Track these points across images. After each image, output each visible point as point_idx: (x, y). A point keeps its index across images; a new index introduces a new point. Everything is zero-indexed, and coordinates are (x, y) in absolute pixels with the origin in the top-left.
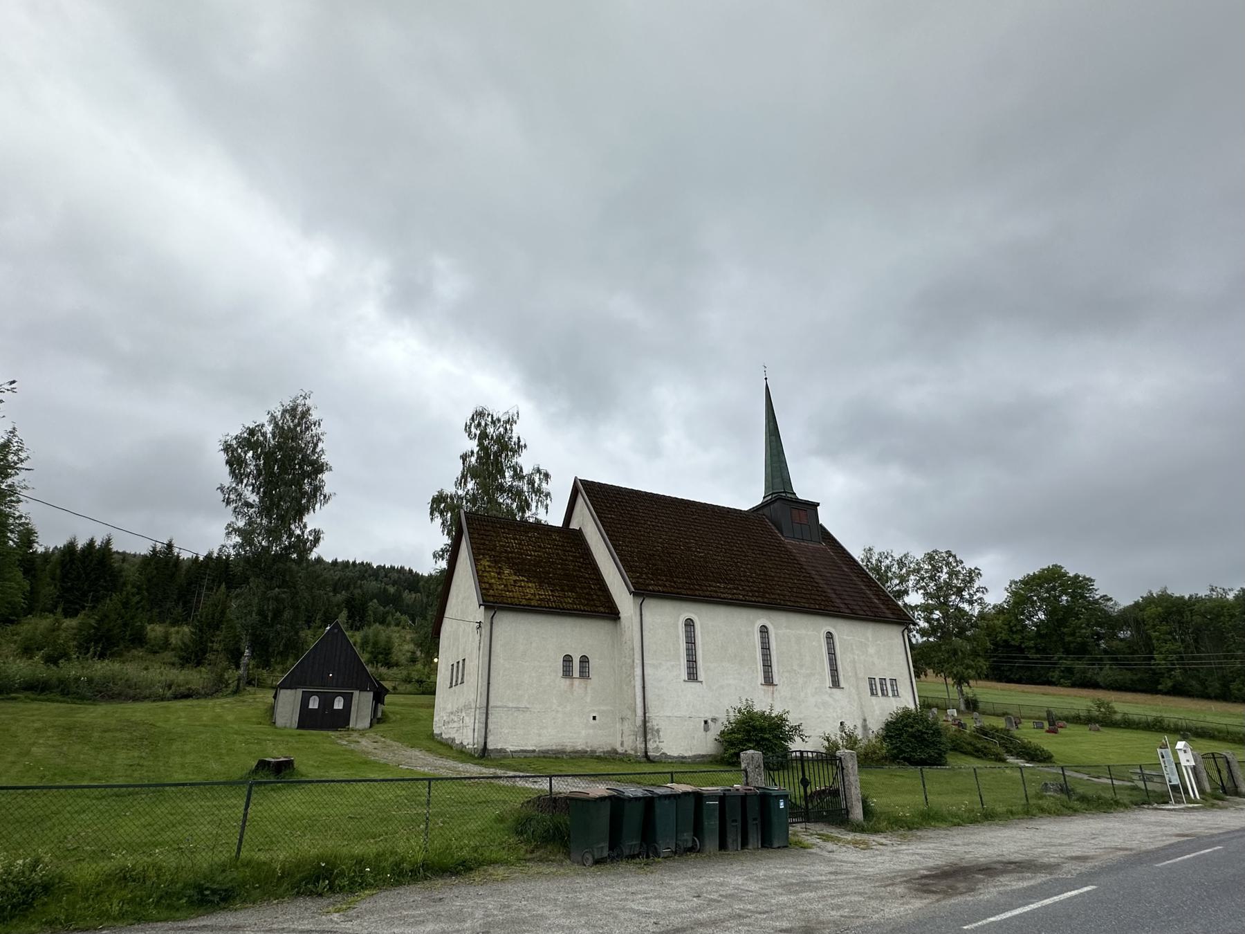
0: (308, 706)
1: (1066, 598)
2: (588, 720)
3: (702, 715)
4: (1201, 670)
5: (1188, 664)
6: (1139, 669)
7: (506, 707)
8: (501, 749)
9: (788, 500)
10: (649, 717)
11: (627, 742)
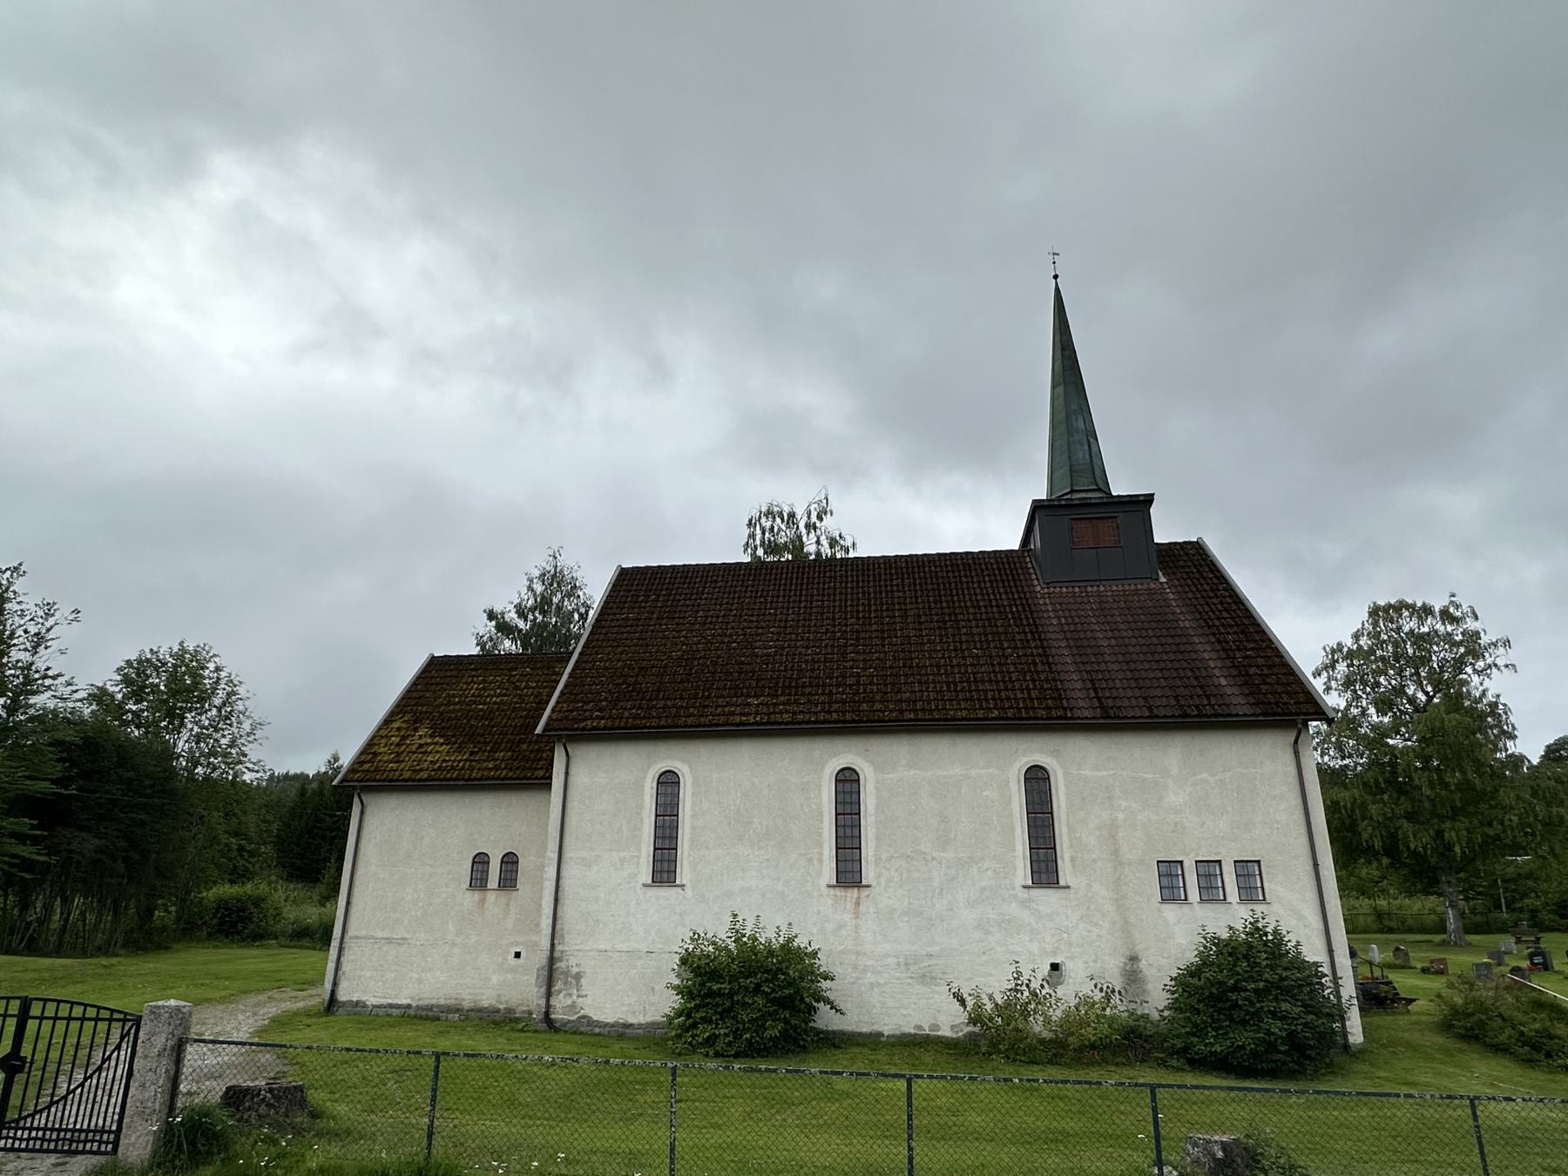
2: (505, 959)
7: (372, 937)
10: (562, 952)
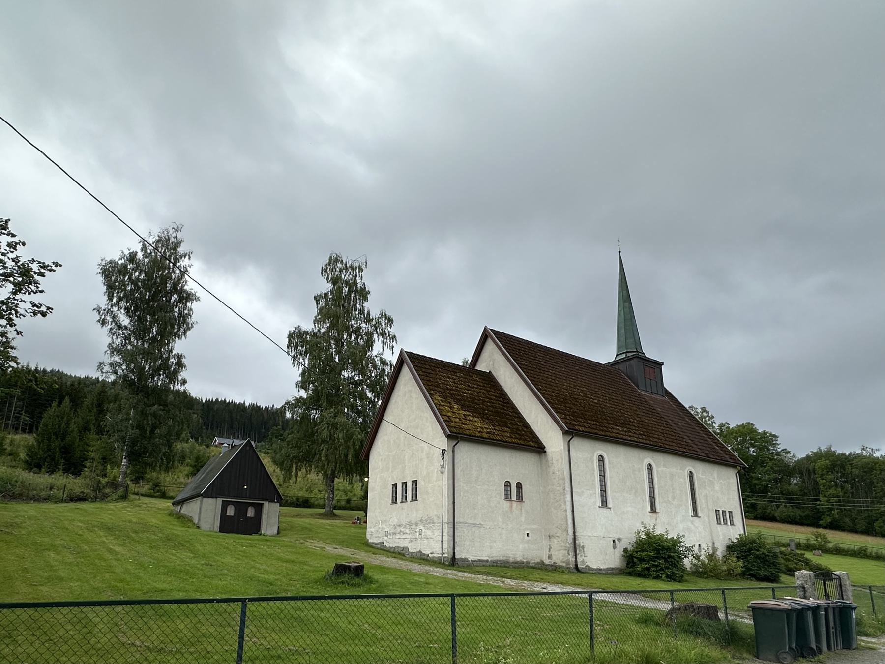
0: (226, 513)
1: (753, 449)
3: (610, 536)
4: (853, 511)
5: (844, 505)
6: (807, 508)
7: (466, 523)
8: (465, 558)
9: (641, 358)
11: (560, 556)
